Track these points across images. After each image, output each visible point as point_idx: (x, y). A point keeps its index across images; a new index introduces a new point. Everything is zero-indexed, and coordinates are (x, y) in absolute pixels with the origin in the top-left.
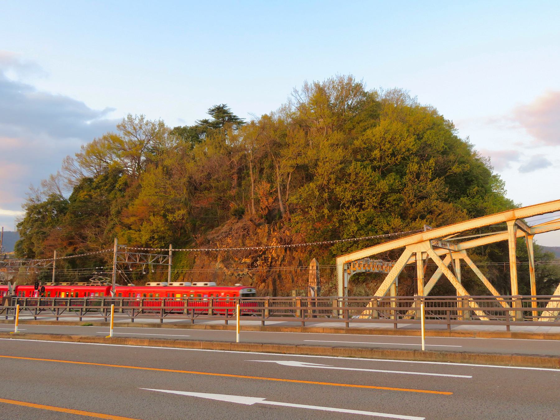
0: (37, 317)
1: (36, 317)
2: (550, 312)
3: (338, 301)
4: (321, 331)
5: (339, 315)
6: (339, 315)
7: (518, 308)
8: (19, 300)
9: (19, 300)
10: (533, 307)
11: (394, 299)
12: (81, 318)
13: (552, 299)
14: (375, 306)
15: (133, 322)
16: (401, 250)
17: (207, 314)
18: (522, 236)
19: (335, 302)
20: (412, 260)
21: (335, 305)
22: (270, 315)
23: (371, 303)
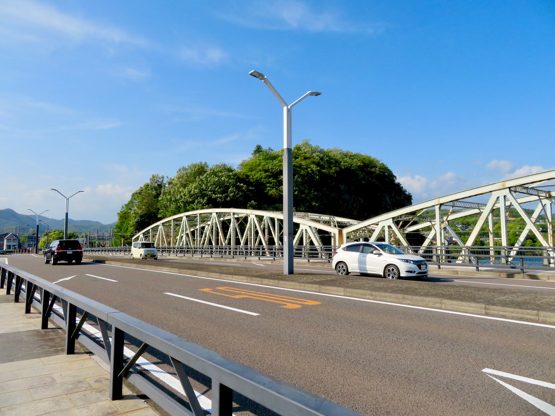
0: (275, 259)
1: (211, 256)
2: (463, 257)
3: (437, 250)
4: (249, 261)
5: (550, 263)
6: (550, 263)
7: (466, 255)
8: (263, 248)
9: (263, 248)
10: (491, 254)
11: (492, 249)
12: (202, 256)
13: (514, 249)
14: (467, 254)
15: (309, 262)
16: (139, 236)
17: (318, 257)
18: (478, 212)
19: (434, 250)
20: (372, 227)
21: (434, 253)
22: (262, 255)
23: (463, 251)
